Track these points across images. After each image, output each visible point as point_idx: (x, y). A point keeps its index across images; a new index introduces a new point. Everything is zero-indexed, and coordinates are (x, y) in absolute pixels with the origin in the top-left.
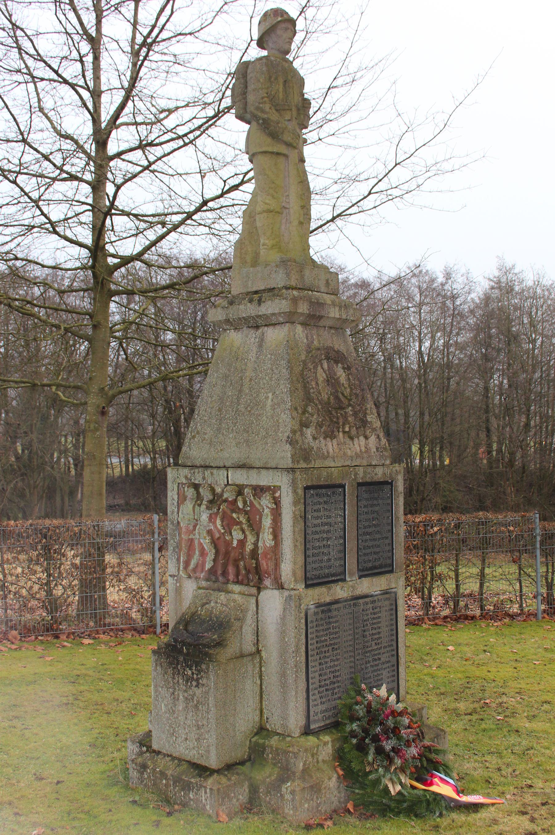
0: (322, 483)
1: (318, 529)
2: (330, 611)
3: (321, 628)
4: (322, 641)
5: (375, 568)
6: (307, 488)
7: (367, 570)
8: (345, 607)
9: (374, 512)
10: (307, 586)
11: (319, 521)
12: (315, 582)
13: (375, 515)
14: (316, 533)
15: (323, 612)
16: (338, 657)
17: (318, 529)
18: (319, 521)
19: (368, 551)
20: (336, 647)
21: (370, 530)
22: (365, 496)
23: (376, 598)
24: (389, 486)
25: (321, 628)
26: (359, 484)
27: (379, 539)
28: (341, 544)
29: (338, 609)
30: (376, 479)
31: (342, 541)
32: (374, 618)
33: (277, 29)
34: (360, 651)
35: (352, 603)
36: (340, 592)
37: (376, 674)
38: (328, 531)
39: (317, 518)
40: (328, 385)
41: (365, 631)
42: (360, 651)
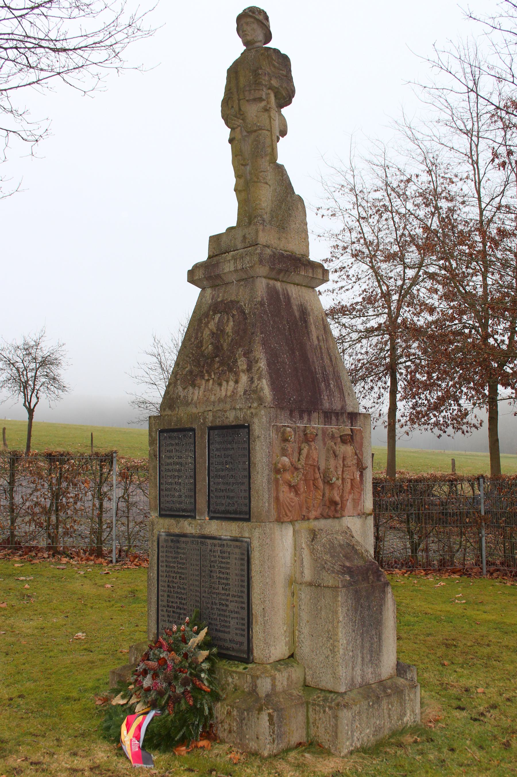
0: (172, 428)
1: (170, 467)
2: (178, 542)
3: (170, 555)
4: (170, 567)
5: (228, 512)
6: (161, 432)
7: (219, 512)
8: (192, 542)
9: (228, 456)
10: (161, 515)
11: (171, 461)
12: (168, 513)
13: (229, 459)
14: (169, 470)
15: (172, 541)
16: (185, 587)
17: (170, 467)
18: (171, 461)
19: (221, 494)
20: (183, 576)
21: (223, 473)
22: (218, 439)
23: (225, 542)
24: (246, 430)
25: (170, 555)
26: (211, 428)
27: (233, 483)
28: (191, 483)
29: (186, 543)
30: (227, 422)
31: (192, 481)
32: (222, 562)
33: (253, 23)
34: (207, 589)
35: (199, 540)
36: (188, 527)
37: (222, 618)
38: (179, 471)
39: (170, 457)
40: (213, 337)
41: (211, 572)
42: (207, 589)
